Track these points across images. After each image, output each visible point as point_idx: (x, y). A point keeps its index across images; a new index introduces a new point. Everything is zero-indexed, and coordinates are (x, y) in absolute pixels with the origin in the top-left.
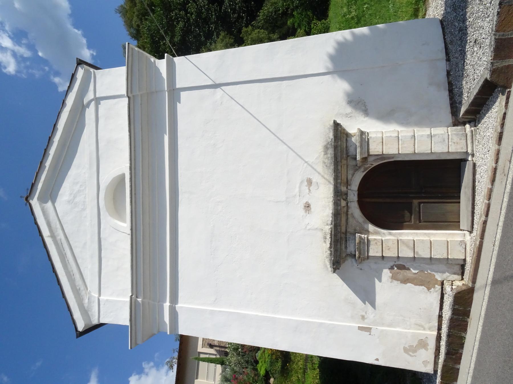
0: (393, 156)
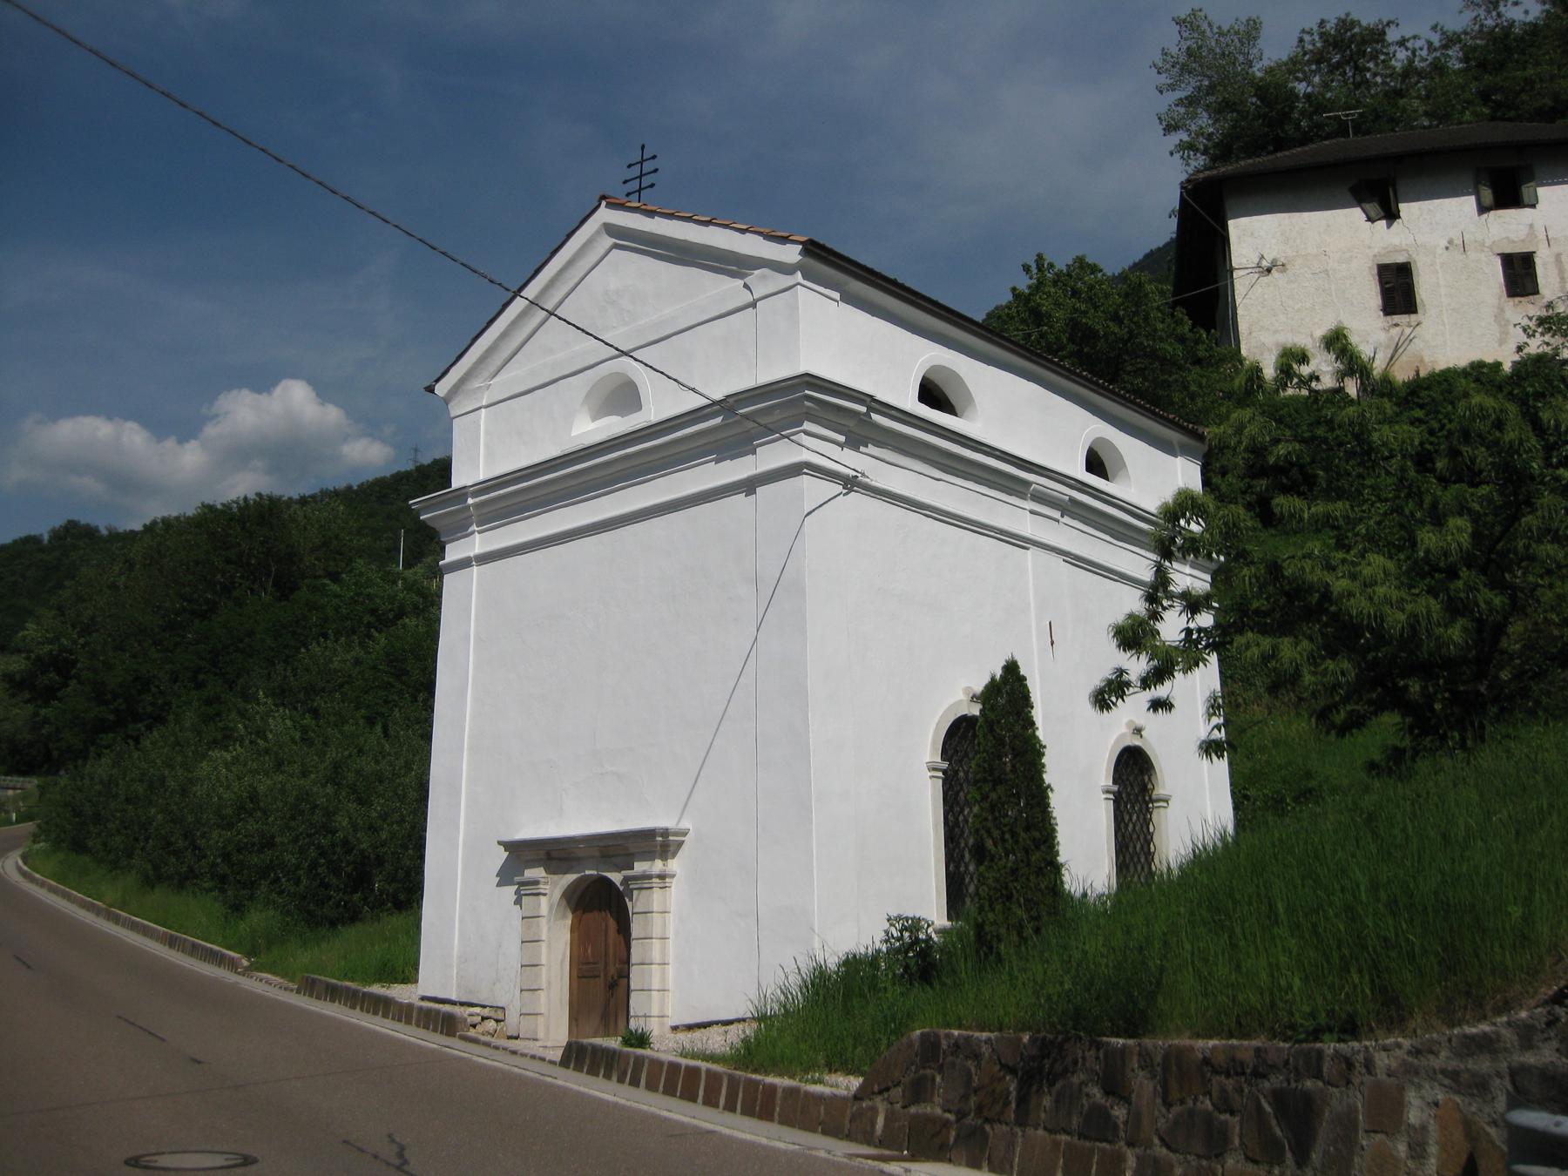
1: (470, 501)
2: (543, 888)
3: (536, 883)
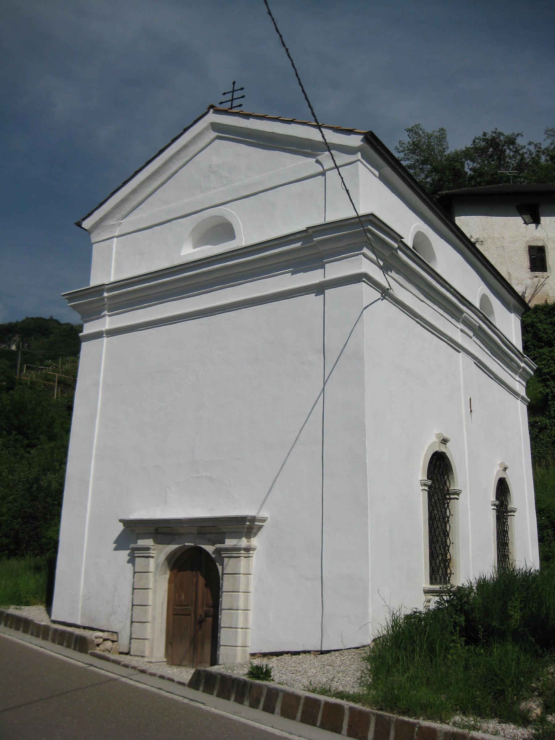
1: (106, 294)
2: (153, 553)
3: (147, 549)
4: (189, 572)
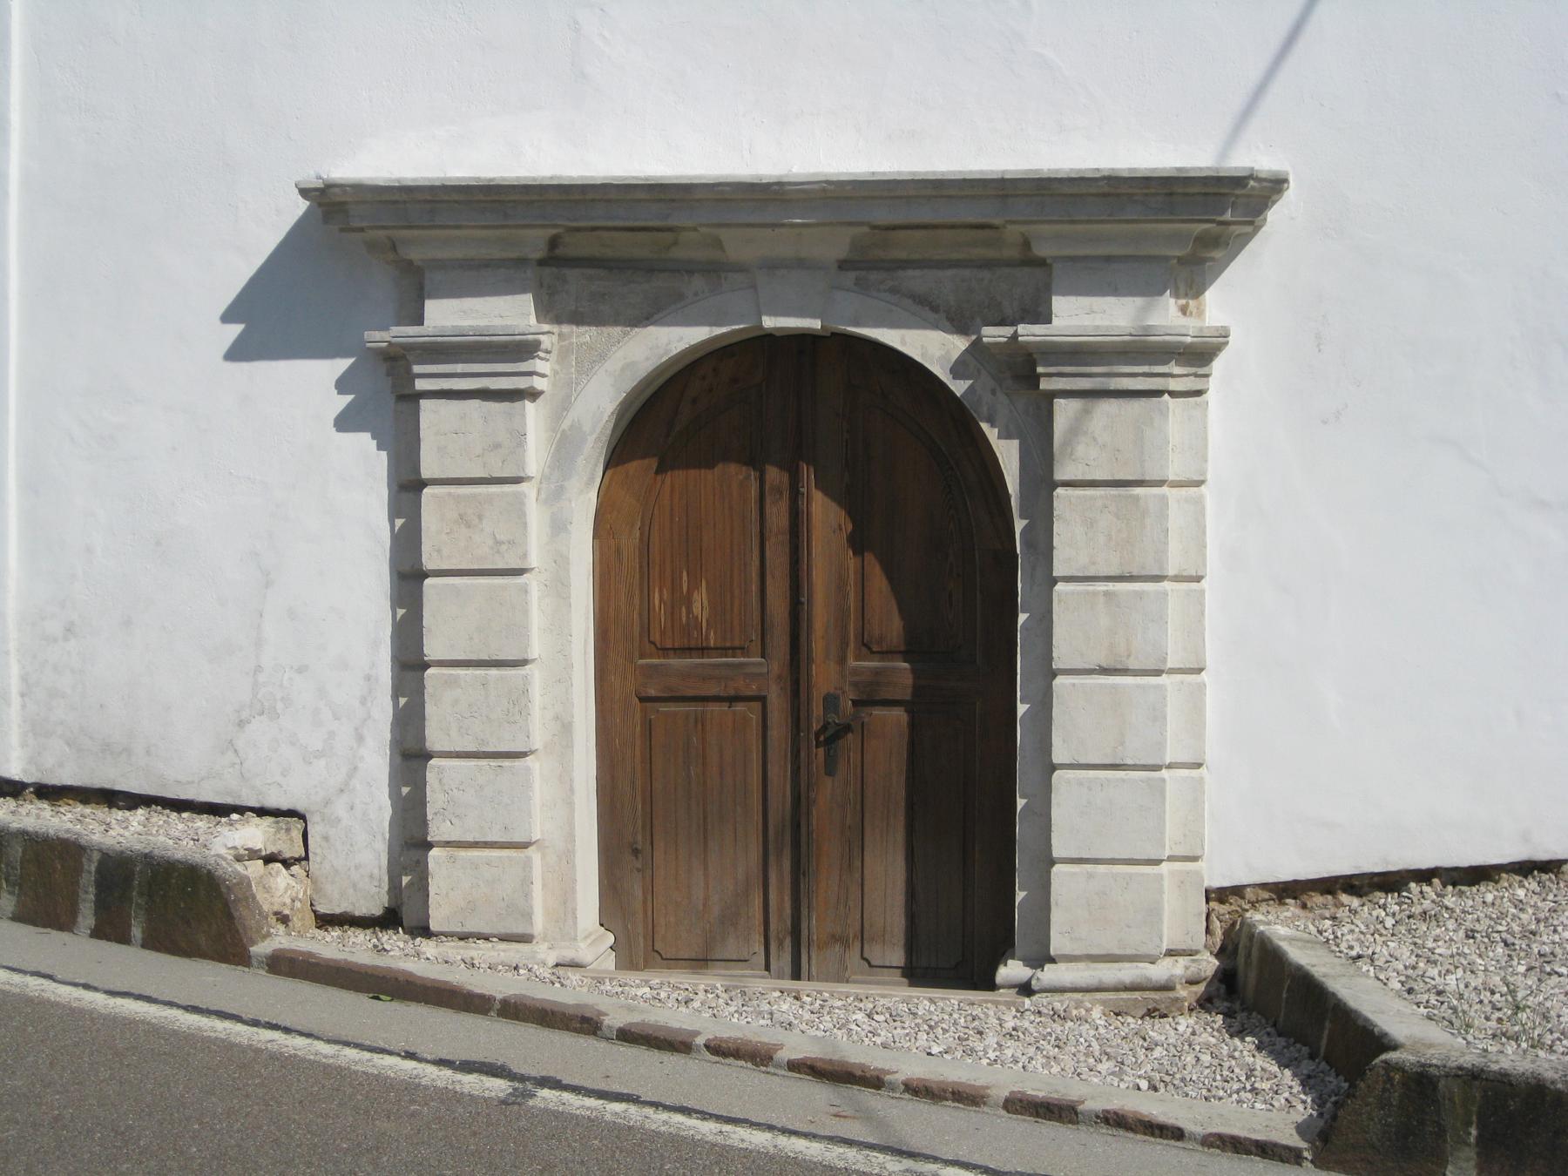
0: (1043, 546)
2: (544, 371)
3: (523, 350)
4: (735, 474)
